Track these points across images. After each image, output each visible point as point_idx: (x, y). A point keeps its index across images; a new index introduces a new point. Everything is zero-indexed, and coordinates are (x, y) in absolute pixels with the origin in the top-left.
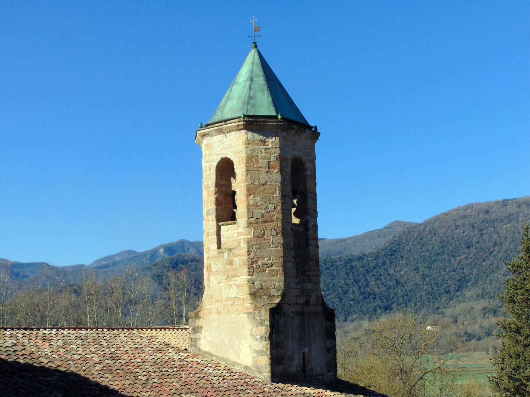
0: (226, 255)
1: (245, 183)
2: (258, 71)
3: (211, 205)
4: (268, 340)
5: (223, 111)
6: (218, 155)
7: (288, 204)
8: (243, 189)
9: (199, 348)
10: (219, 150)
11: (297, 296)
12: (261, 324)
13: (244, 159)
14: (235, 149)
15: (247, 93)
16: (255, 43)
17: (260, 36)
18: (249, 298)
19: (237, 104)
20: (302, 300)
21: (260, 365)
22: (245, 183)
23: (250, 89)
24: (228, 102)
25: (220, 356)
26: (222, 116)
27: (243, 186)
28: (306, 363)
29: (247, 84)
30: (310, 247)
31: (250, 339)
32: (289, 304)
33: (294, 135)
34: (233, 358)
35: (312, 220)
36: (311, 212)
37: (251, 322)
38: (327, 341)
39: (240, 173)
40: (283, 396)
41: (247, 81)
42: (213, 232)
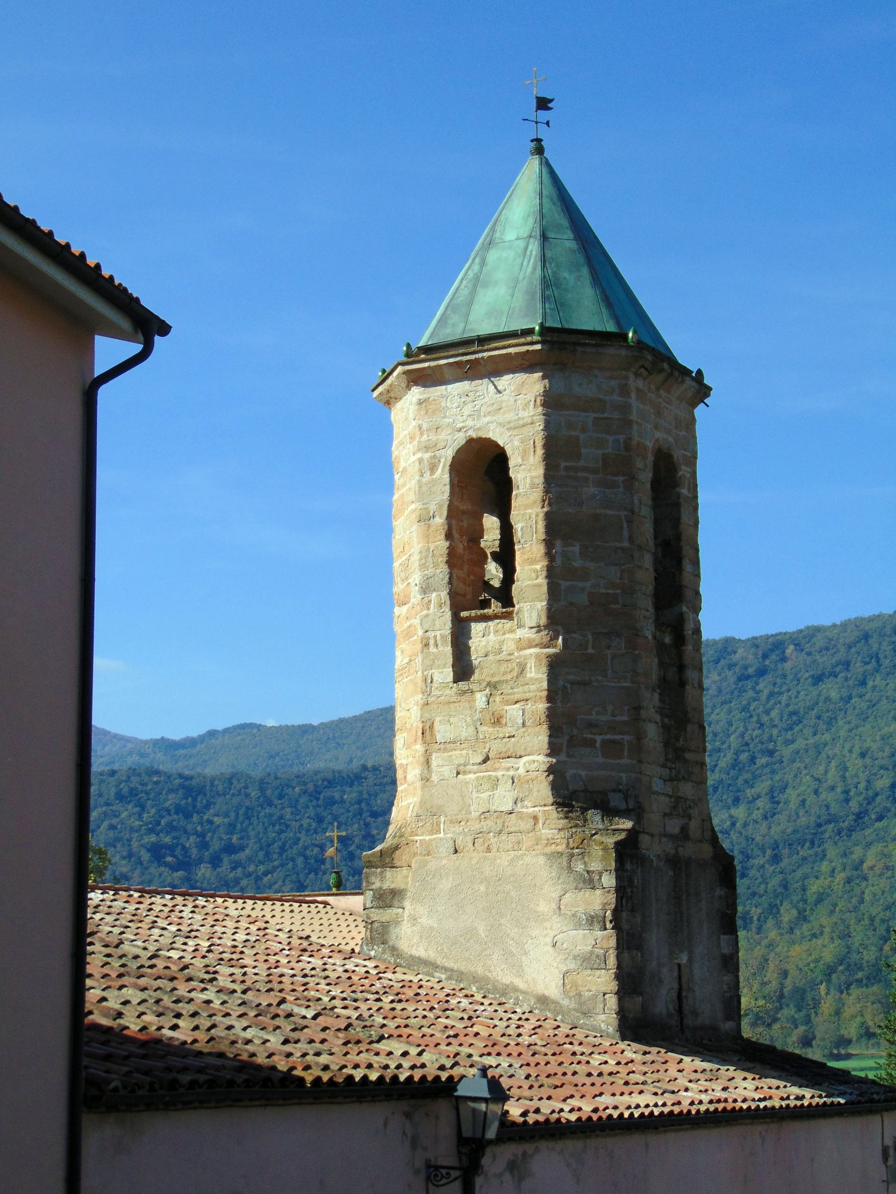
0: (480, 699)
1: (543, 507)
2: (556, 216)
3: (435, 566)
4: (609, 925)
5: (467, 315)
6: (460, 430)
7: (647, 569)
8: (536, 523)
9: (394, 949)
10: (461, 419)
11: (665, 815)
12: (589, 881)
13: (540, 444)
14: (511, 416)
15: (534, 269)
16: (539, 141)
17: (548, 123)
18: (555, 815)
19: (509, 298)
20: (674, 826)
21: (586, 994)
22: (543, 507)
23: (544, 260)
24: (480, 291)
25: (463, 968)
26: (468, 327)
27: (537, 516)
28: (684, 994)
29: (530, 247)
30: (687, 687)
31: (556, 924)
32: (652, 835)
33: (658, 389)
34: (504, 976)
35: (691, 616)
36: (688, 593)
37: (559, 878)
38: (722, 937)
39: (528, 481)
40: (558, 1089)
41: (532, 240)
42: (442, 636)
